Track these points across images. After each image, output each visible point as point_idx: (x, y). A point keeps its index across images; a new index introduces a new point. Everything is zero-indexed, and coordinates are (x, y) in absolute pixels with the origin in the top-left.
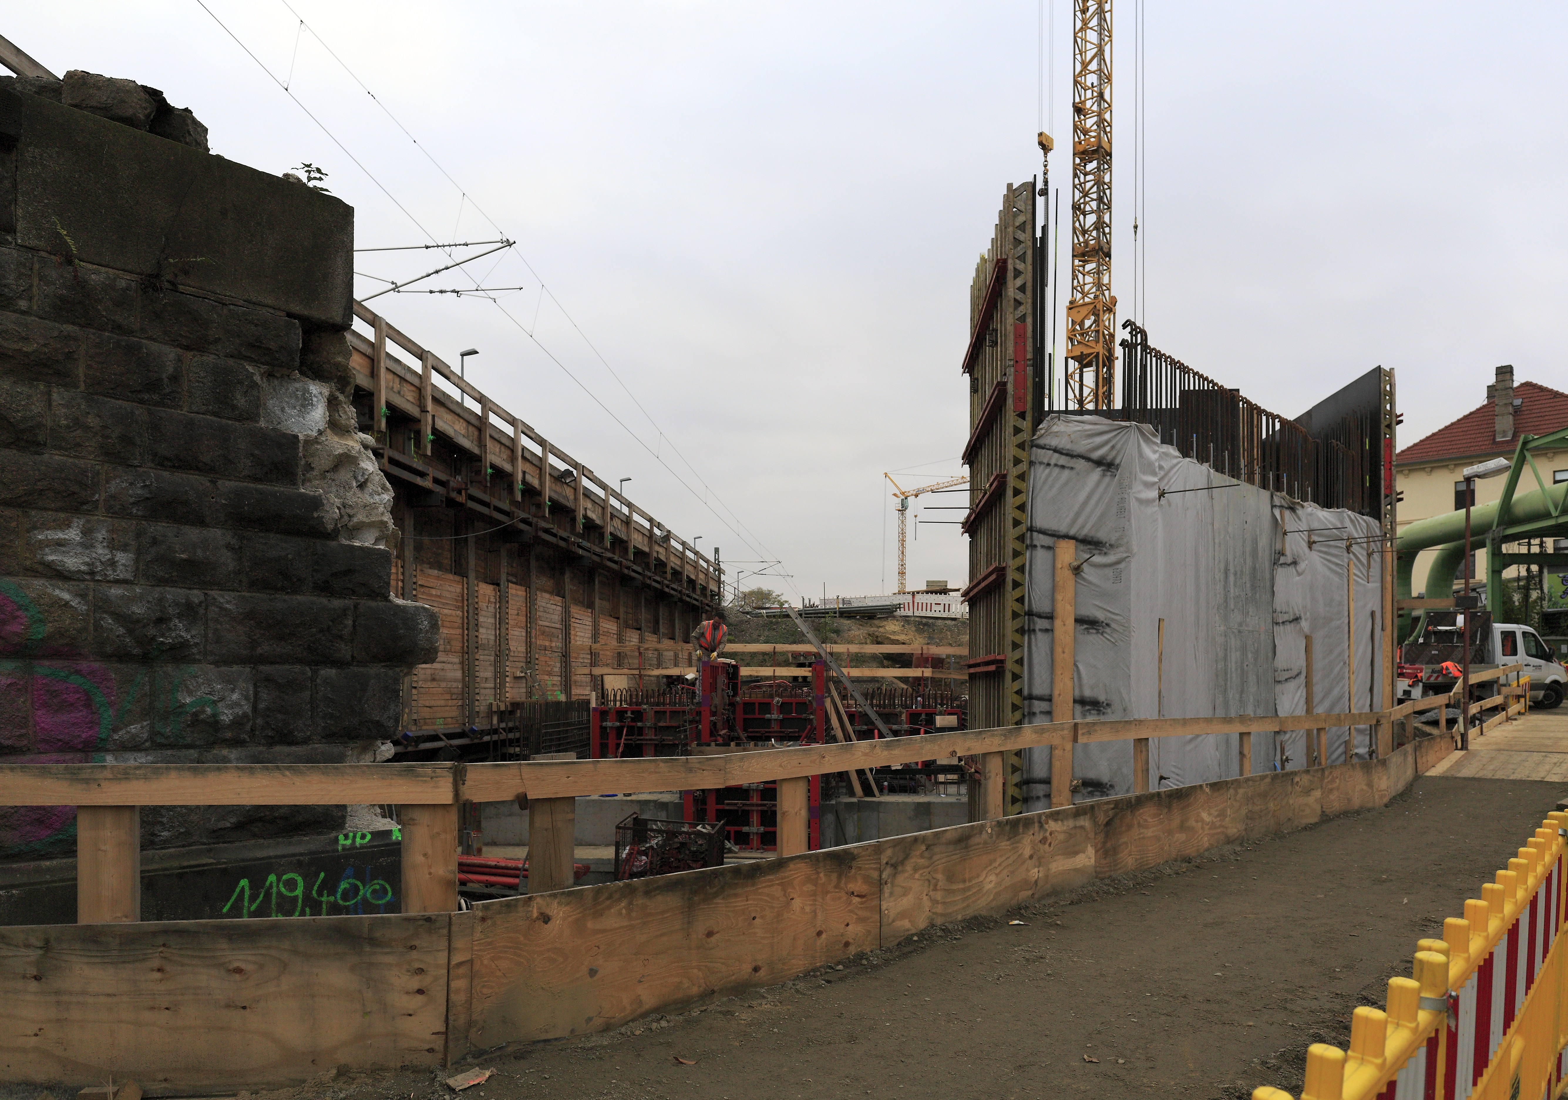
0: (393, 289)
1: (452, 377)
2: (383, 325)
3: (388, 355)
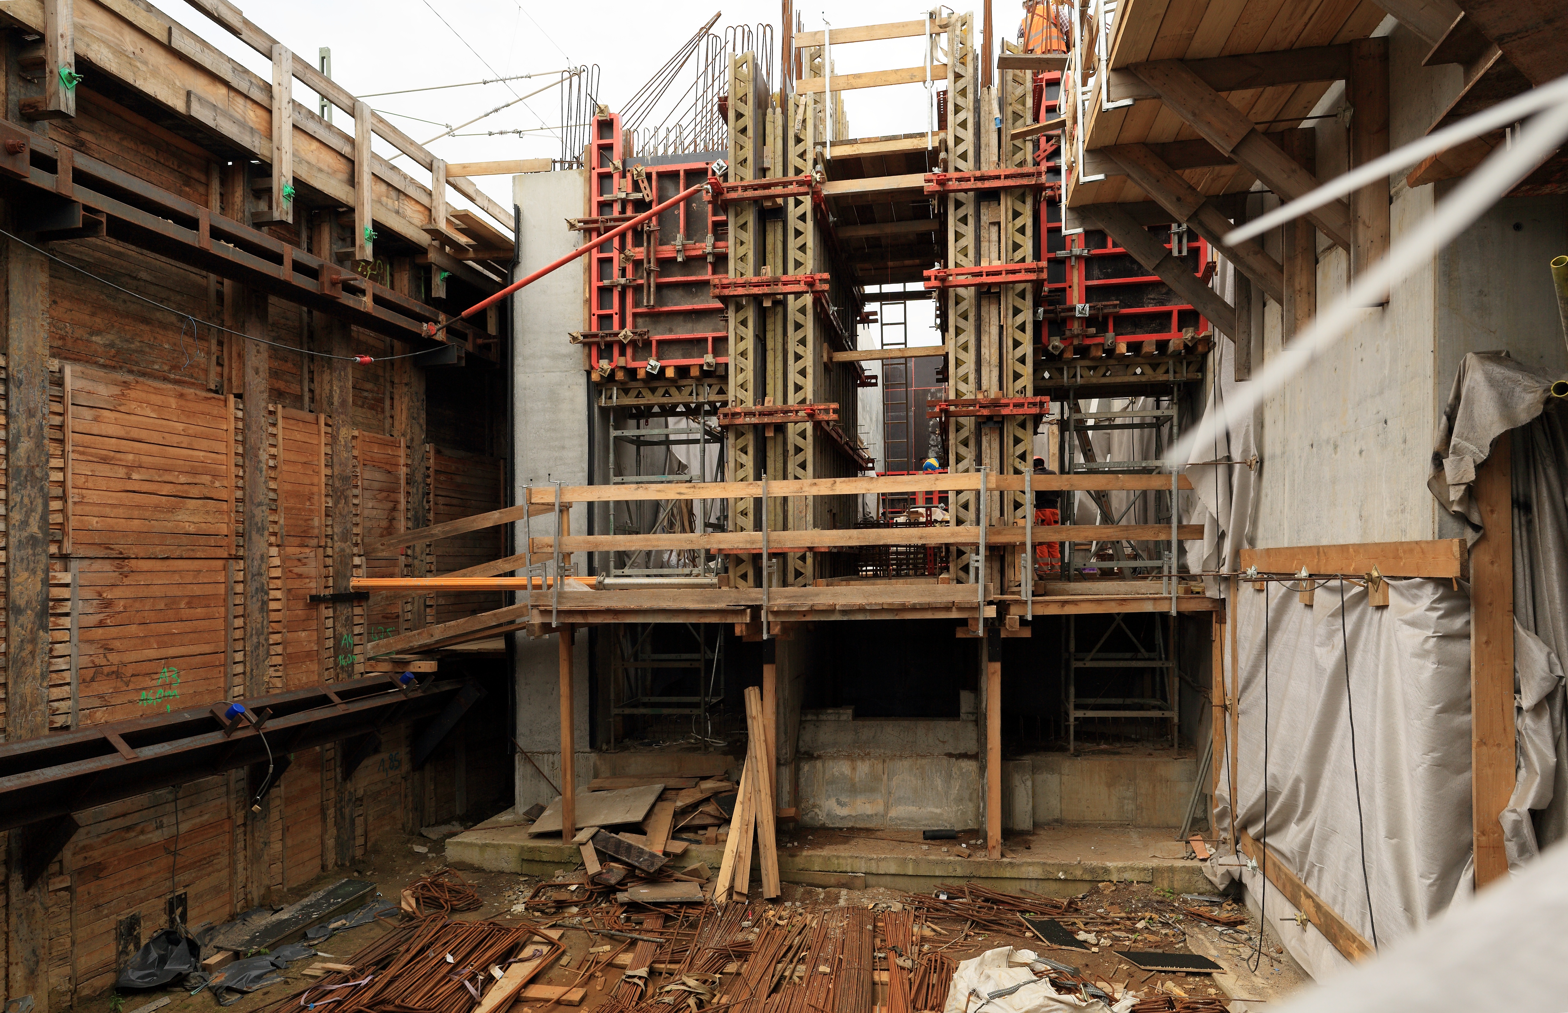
0: (448, 133)
1: (479, 200)
2: (367, 114)
3: (375, 156)
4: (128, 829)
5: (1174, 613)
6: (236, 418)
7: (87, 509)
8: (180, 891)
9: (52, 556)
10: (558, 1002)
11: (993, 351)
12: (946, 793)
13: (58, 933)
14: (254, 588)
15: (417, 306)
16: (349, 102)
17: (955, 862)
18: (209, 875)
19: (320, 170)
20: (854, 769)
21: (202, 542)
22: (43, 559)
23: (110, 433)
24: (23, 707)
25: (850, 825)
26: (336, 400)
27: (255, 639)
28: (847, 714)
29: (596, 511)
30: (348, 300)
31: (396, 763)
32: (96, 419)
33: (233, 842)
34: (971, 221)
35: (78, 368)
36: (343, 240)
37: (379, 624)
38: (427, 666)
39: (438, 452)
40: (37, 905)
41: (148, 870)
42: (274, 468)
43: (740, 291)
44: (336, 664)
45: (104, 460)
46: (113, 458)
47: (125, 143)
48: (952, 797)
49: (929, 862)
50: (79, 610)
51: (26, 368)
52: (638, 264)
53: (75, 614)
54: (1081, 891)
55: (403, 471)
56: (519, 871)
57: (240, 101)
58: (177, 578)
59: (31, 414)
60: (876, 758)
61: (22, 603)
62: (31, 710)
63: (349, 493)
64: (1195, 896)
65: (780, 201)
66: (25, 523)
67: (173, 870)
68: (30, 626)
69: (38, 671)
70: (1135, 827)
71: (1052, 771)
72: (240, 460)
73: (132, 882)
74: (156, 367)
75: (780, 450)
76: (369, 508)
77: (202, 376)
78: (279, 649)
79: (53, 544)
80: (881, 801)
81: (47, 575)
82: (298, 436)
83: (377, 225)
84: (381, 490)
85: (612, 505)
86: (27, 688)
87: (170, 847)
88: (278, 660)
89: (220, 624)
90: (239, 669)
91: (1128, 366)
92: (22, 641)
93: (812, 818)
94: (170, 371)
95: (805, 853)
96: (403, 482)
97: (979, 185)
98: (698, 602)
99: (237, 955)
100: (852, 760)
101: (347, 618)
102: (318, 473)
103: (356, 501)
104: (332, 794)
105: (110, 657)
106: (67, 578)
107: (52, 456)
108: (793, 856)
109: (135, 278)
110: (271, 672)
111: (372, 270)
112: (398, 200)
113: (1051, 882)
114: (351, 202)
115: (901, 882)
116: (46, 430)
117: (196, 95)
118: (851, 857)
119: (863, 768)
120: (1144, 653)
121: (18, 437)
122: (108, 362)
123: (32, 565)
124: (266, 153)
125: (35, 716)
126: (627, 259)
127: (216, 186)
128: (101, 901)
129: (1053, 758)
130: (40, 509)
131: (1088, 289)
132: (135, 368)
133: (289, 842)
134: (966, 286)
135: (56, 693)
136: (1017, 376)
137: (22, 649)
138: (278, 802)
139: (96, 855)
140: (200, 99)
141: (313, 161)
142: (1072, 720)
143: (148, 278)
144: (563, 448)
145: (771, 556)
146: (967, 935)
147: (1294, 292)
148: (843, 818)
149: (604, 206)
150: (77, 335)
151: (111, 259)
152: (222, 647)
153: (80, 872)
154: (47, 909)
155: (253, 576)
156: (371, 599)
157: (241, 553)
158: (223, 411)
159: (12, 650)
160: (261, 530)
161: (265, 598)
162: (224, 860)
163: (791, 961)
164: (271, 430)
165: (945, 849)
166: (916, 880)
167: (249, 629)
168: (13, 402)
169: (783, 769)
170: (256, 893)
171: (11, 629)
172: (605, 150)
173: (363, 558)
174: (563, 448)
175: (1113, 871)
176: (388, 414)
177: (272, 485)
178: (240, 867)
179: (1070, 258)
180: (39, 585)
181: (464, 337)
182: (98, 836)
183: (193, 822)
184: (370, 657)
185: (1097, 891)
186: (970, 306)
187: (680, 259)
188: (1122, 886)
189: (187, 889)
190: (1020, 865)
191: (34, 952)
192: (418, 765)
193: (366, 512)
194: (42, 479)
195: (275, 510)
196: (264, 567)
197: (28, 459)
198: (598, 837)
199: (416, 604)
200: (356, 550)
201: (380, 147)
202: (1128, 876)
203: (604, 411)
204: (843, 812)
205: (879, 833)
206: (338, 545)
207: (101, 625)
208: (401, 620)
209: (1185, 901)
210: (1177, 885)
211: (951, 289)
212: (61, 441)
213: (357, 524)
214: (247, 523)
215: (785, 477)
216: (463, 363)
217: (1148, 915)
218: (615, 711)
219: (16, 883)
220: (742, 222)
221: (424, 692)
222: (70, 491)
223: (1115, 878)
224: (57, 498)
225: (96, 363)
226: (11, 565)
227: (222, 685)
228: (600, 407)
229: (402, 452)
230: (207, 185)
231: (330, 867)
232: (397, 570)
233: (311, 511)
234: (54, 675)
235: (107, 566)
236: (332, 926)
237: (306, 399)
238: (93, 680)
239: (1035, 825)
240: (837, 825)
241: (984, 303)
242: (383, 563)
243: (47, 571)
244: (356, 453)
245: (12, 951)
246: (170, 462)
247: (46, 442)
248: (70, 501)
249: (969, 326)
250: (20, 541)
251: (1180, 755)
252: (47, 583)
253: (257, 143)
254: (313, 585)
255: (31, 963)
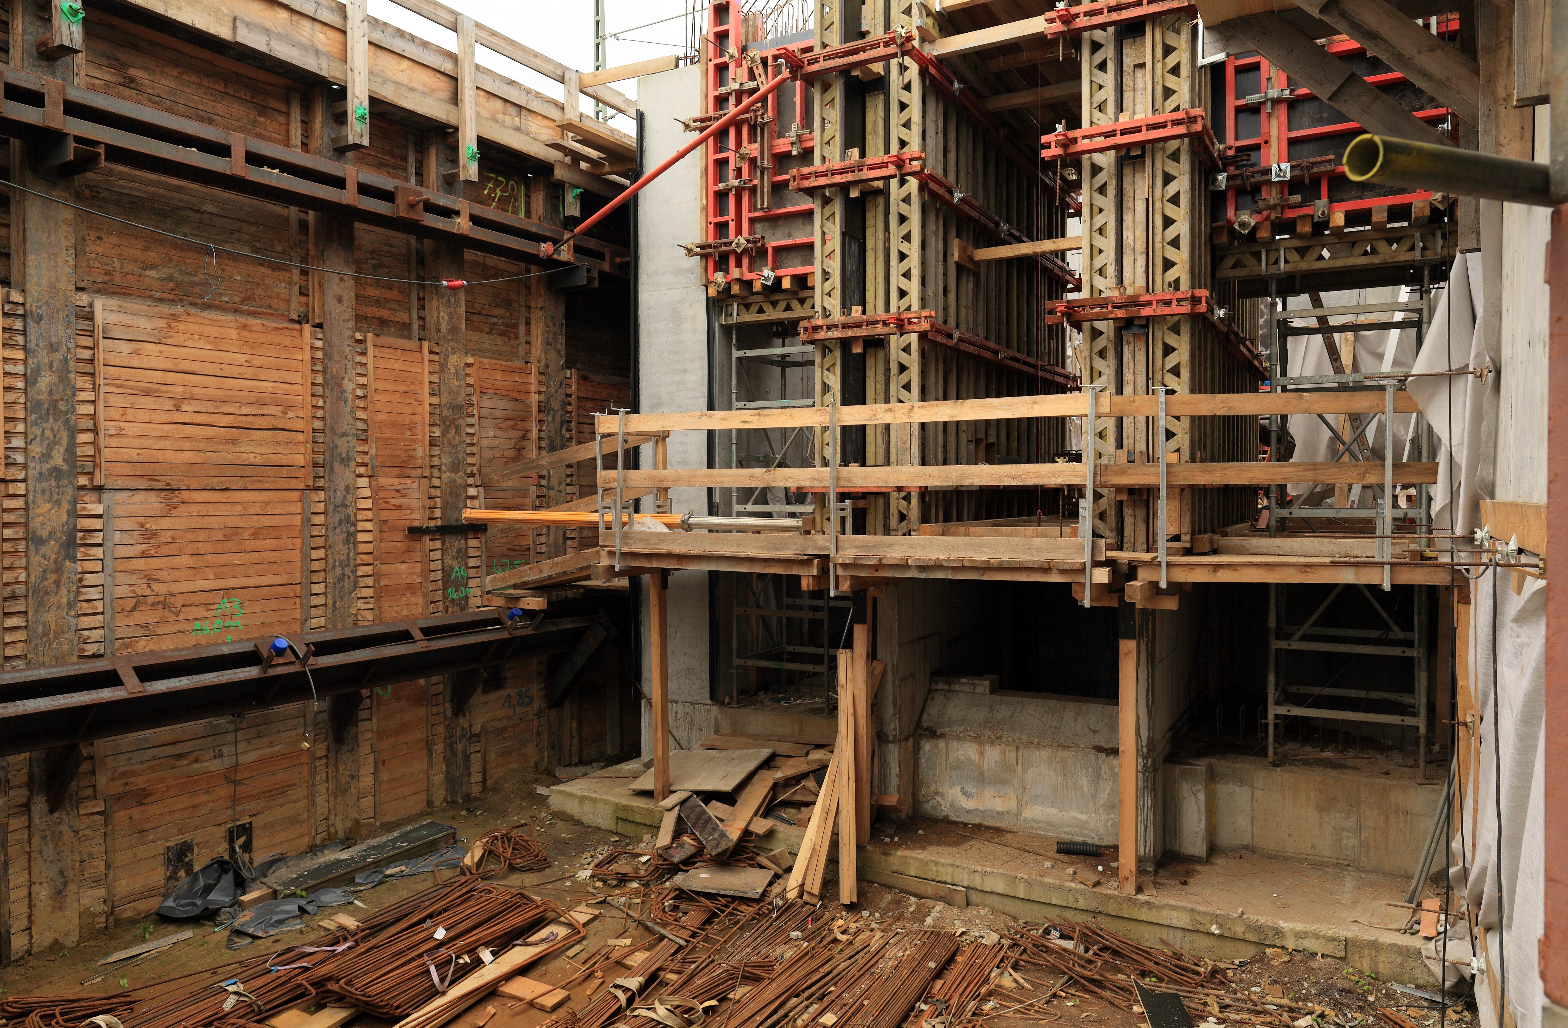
4: (179, 756)
5: (1387, 587)
6: (313, 348)
7: (126, 442)
8: (245, 820)
9: (82, 488)
10: (531, 1004)
11: (1138, 233)
12: (1094, 797)
13: (91, 856)
14: (337, 520)
16: (451, 18)
17: (1077, 891)
18: (282, 805)
19: (412, 89)
20: (982, 754)
21: (270, 474)
22: (70, 491)
23: (154, 366)
24: (45, 634)
25: (977, 821)
26: (444, 327)
27: (338, 571)
28: (983, 685)
29: (717, 440)
31: (526, 700)
32: (136, 353)
33: (313, 773)
34: (1111, 66)
35: (114, 302)
37: (503, 556)
38: (534, 603)
39: (584, 378)
40: (64, 828)
41: (203, 798)
42: (365, 397)
43: (822, 181)
44: (445, 598)
45: (147, 393)
46: (157, 391)
47: (185, 77)
48: (1101, 802)
49: (1044, 885)
50: (123, 541)
51: (47, 303)
52: (753, 161)
53: (108, 544)
54: (1233, 956)
55: (534, 398)
56: (614, 829)
57: (307, 24)
58: (238, 509)
59: (53, 348)
60: (1008, 743)
61: (45, 534)
62: (56, 638)
63: (461, 422)
64: (1410, 989)
65: (878, 68)
66: (47, 456)
67: (235, 800)
68: (53, 556)
69: (64, 601)
70: (1358, 869)
71: (1241, 782)
72: (319, 390)
73: (184, 809)
74: (225, 299)
75: (881, 369)
76: (491, 438)
77: (283, 306)
78: (370, 581)
79: (81, 475)
80: (1013, 796)
81: (75, 507)
82: (396, 366)
83: (482, 142)
84: (505, 419)
85: (734, 434)
86: (51, 617)
87: (231, 777)
88: (370, 592)
89: (296, 555)
90: (320, 600)
91: (1353, 244)
92: (44, 571)
93: (934, 808)
94: (242, 303)
95: (900, 853)
96: (534, 410)
97: (1115, 16)
98: (763, 548)
99: (275, 894)
100: (980, 744)
101: (459, 551)
102: (421, 402)
103: (469, 430)
104: (441, 729)
105: (155, 587)
106: (99, 509)
107: (81, 389)
108: (886, 854)
109: (198, 211)
110: (361, 604)
111: (502, 191)
112: (519, 115)
113: (1202, 936)
114: (453, 121)
115: (1011, 906)
116: (72, 364)
117: (243, 21)
118: (952, 865)
119: (993, 754)
120: (1397, 633)
121: (37, 372)
122: (165, 296)
123: (55, 497)
124: (341, 76)
125: (61, 644)
126: (742, 157)
127: (296, 114)
128: (146, 826)
129: (1243, 765)
130: (65, 442)
131: (1292, 142)
132: (199, 301)
133: (385, 776)
134: (1101, 150)
135: (86, 622)
136: (1168, 264)
137: (44, 577)
138: (369, 735)
139: (140, 781)
140: (248, 24)
141: (405, 81)
142: (1271, 717)
143: (215, 211)
144: (685, 371)
145: (842, 497)
146: (1054, 996)
147: (1496, 101)
148: (969, 812)
149: (721, 101)
150: (125, 270)
151: (168, 194)
152: (297, 578)
153: (119, 798)
154: (77, 832)
155: (336, 507)
156: (489, 531)
157: (321, 483)
158: (298, 341)
159: (32, 579)
160: (346, 461)
161: (352, 529)
162: (303, 792)
163: (807, 999)
164: (358, 359)
165: (1070, 870)
166: (1028, 906)
167: (331, 561)
168: (32, 337)
170: (340, 826)
171: (32, 559)
172: (722, 37)
173: (481, 489)
174: (685, 371)
175: (1288, 934)
176: (522, 339)
177: (361, 415)
178: (320, 800)
179: (1264, 103)
180: (65, 517)
181: (601, 256)
182: (142, 762)
183: (262, 752)
184: (486, 591)
185: (1261, 959)
186: (1110, 177)
187: (794, 153)
188: (1298, 957)
189: (253, 819)
190: (1161, 907)
191: (61, 873)
192: (555, 701)
193: (485, 442)
194: (67, 412)
195: (366, 441)
196: (350, 498)
197: (51, 393)
198: (688, 804)
199: (552, 537)
200: (470, 481)
201: (485, 57)
202: (1309, 945)
203: (727, 330)
204: (969, 804)
205: (1009, 836)
206: (447, 476)
207: (143, 555)
208: (532, 552)
209: (1390, 995)
210: (1384, 969)
211: (1085, 157)
212: (92, 375)
214: (327, 454)
215: (887, 400)
216: (596, 284)
217: (1318, 1009)
218: (737, 662)
219: (40, 805)
220: (829, 99)
221: (535, 629)
222: (102, 424)
223: (1290, 944)
224: (88, 430)
225: (150, 297)
226: (31, 497)
227: (298, 616)
228: (722, 326)
229: (533, 379)
230: (288, 114)
231: (437, 803)
232: (528, 501)
233: (414, 441)
234: (84, 605)
235: (152, 497)
236: (389, 872)
237: (415, 326)
238: (134, 609)
239: (1213, 850)
240: (962, 819)
241: (1127, 171)
242: (510, 494)
243: (74, 502)
244: (470, 380)
245: (35, 870)
246: (230, 393)
247: (72, 375)
248: (102, 434)
249: (1108, 202)
250: (40, 474)
251: (1429, 779)
252: (74, 514)
253: (324, 66)
254: (416, 516)
255: (58, 884)
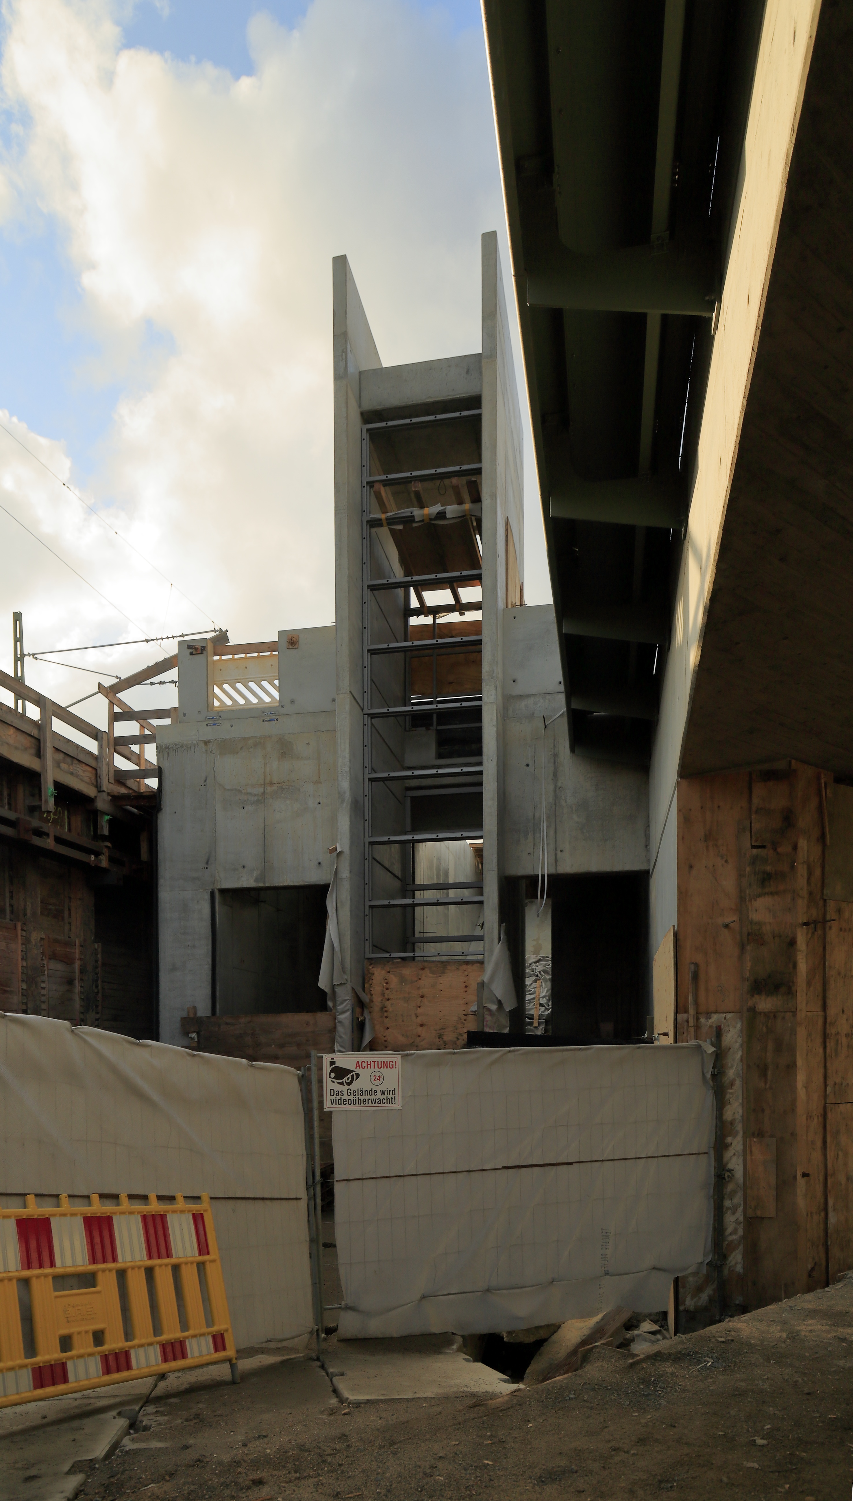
15: (86, 842)
19: (16, 748)
26: (29, 912)
30: (37, 841)
36: (33, 795)
55: (77, 965)
83: (57, 785)
103: (43, 985)
169: (227, 1366)
201: (59, 726)
213: (44, 1002)
